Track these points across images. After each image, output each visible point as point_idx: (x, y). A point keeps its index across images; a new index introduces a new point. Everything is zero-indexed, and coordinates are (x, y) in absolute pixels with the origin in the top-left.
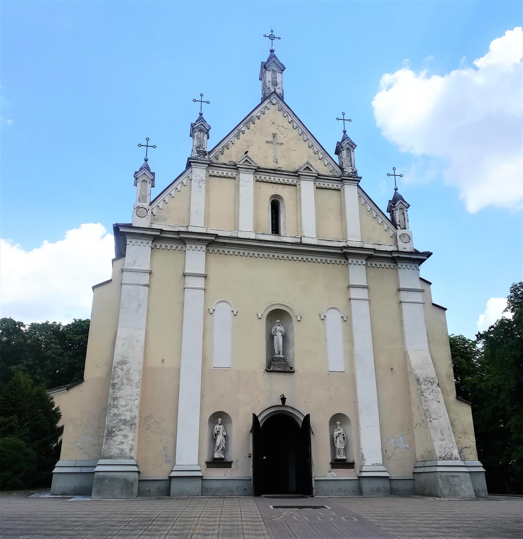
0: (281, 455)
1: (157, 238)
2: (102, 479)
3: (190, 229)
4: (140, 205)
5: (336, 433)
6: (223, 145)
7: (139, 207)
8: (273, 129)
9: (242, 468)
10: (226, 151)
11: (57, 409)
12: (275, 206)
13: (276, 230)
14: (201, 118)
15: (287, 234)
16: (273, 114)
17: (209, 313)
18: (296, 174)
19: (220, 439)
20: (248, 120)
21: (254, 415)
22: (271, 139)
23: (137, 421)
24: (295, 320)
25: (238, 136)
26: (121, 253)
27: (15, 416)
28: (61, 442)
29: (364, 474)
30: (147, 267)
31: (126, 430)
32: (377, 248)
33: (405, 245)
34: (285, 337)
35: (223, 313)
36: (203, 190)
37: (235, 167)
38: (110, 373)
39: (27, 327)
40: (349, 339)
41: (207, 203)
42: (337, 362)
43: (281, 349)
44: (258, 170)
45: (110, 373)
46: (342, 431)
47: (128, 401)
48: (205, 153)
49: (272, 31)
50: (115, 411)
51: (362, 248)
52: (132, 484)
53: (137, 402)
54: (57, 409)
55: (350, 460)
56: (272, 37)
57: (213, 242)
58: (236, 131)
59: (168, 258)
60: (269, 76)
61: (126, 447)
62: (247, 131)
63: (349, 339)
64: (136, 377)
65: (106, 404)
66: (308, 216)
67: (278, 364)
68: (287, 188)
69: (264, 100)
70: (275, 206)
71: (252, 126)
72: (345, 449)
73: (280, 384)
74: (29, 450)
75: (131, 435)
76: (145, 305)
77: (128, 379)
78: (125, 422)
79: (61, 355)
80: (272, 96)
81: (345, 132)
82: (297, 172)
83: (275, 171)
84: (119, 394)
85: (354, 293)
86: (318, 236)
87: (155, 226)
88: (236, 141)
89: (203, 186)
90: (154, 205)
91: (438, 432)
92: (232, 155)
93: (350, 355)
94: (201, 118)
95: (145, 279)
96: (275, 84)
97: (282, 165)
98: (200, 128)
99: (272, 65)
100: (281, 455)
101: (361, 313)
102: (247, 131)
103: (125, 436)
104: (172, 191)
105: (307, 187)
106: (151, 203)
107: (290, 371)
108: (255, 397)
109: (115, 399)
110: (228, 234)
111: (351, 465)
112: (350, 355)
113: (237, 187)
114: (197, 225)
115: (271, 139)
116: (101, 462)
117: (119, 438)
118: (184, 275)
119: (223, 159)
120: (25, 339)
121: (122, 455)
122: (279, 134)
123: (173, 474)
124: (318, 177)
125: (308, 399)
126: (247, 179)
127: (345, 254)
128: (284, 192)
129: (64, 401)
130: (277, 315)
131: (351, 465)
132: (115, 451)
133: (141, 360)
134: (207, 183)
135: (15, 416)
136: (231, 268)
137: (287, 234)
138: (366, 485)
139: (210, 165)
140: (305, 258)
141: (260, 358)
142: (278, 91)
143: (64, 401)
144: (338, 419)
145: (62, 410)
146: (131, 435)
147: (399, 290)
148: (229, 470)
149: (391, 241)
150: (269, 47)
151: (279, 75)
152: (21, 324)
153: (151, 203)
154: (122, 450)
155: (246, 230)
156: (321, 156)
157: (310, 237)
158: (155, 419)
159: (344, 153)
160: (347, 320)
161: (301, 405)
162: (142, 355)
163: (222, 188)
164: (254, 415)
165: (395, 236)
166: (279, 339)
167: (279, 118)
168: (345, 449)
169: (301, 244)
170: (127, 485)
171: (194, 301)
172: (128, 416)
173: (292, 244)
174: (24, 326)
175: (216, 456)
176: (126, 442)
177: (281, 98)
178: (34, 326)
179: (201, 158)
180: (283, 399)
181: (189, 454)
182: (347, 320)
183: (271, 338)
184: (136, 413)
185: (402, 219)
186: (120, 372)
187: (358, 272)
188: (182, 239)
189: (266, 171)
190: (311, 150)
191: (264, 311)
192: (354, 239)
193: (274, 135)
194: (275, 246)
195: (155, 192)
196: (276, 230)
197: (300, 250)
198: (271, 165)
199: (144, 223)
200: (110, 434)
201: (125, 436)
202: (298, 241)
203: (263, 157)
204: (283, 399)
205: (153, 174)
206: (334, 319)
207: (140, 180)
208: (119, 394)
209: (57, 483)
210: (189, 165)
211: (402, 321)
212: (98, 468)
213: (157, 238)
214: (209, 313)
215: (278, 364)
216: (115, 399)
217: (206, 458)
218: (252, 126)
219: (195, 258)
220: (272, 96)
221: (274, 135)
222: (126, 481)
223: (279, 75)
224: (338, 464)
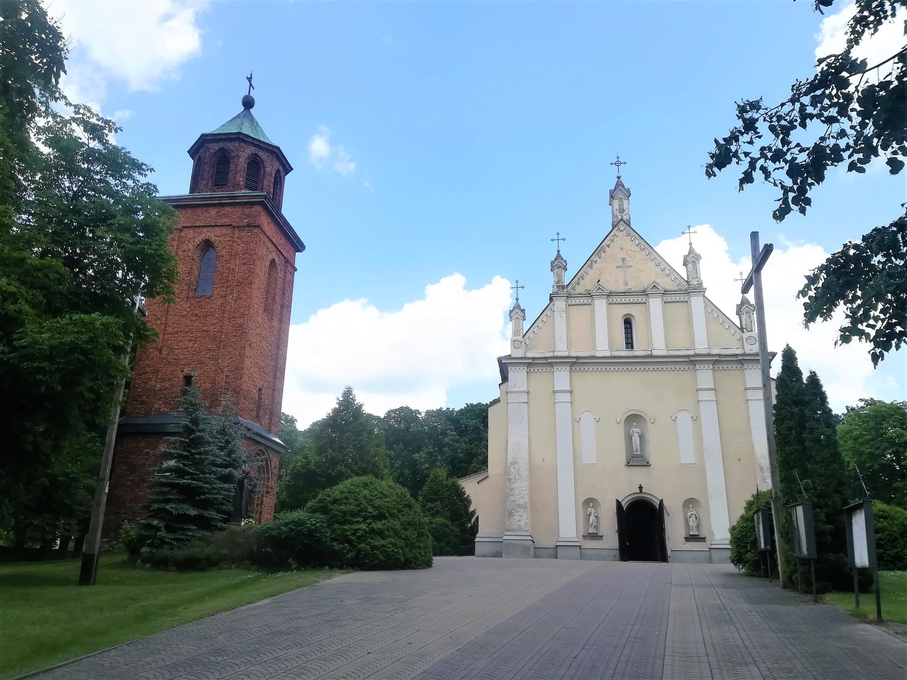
0: (641, 529)
1: (531, 364)
2: (509, 545)
3: (556, 354)
4: (516, 338)
5: (689, 514)
6: (578, 276)
7: (515, 341)
8: (622, 255)
9: (611, 540)
10: (581, 281)
11: (468, 496)
12: (628, 323)
13: (629, 344)
14: (559, 256)
15: (639, 349)
16: (622, 240)
17: (576, 421)
18: (644, 293)
19: (592, 518)
20: (599, 250)
21: (617, 501)
22: (620, 264)
23: (528, 505)
24: (649, 423)
25: (591, 266)
26: (505, 379)
27: (439, 503)
28: (478, 518)
29: (713, 546)
30: (525, 389)
31: (521, 512)
32: (724, 352)
33: (751, 347)
34: (641, 437)
35: (587, 420)
36: (564, 319)
37: (589, 295)
38: (506, 472)
39: (423, 415)
40: (698, 435)
41: (568, 330)
42: (688, 456)
43: (638, 447)
44: (610, 294)
45: (506, 472)
46: (694, 512)
47: (521, 490)
48: (563, 287)
49: (618, 157)
50: (512, 498)
51: (709, 355)
52: (529, 549)
53: (527, 492)
54: (468, 496)
55: (703, 536)
56: (618, 164)
57: (575, 363)
58: (589, 262)
59: (540, 378)
60: (616, 203)
61: (522, 523)
62: (599, 260)
63: (698, 435)
64: (525, 474)
65: (506, 494)
66: (655, 337)
67: (637, 459)
68: (638, 307)
69: (614, 227)
70: (628, 323)
71: (603, 255)
72: (698, 527)
73: (639, 476)
74: (454, 528)
75: (525, 515)
76: (526, 418)
77: (519, 475)
78: (520, 506)
79: (458, 441)
80: (621, 223)
81: (690, 244)
82: (644, 291)
83: (625, 293)
84: (514, 486)
85: (702, 396)
86: (667, 346)
87: (529, 355)
88: (590, 271)
89: (564, 315)
90: (526, 337)
91: (225, 502)
92: (587, 284)
93: (700, 451)
94: (559, 256)
95: (524, 398)
96: (622, 211)
97: (633, 286)
98: (559, 264)
99: (619, 192)
100: (641, 529)
101: (709, 413)
102: (599, 260)
103: (521, 516)
104: (539, 323)
105: (655, 303)
106: (524, 336)
107: (648, 465)
108: (622, 487)
109: (512, 490)
110: (587, 354)
111: (703, 539)
112: (700, 451)
113: (593, 311)
114: (562, 350)
115: (620, 264)
116: (506, 533)
117: (517, 518)
118: (554, 392)
119: (580, 289)
120: (422, 426)
121: (520, 529)
122: (628, 258)
123: (558, 544)
124: (666, 292)
125: (661, 488)
126: (600, 305)
127: (692, 361)
128: (636, 312)
129: (469, 486)
130: (634, 419)
131: (703, 539)
132: (515, 526)
133: (527, 461)
134: (567, 311)
135: (439, 503)
136: (592, 383)
137: (639, 349)
138: (715, 555)
139: (569, 297)
140: (656, 368)
141: (621, 457)
142: (625, 218)
143: (469, 486)
144: (690, 503)
145: (472, 498)
146: (525, 515)
147: (746, 389)
148: (601, 542)
149: (739, 345)
150: (617, 174)
151: (625, 202)
152: (418, 412)
153: (524, 336)
154: (520, 525)
155: (602, 349)
156: (668, 272)
157: (660, 348)
158: (542, 504)
159: (690, 265)
160: (696, 419)
161: (656, 492)
162: (527, 458)
163: (581, 314)
164: (617, 501)
165: (741, 339)
166: (636, 439)
167: (629, 244)
168: (698, 527)
169: (651, 356)
170: (526, 549)
171: (563, 411)
172: (522, 502)
173: (643, 357)
174: (420, 414)
175: (590, 531)
176: (522, 520)
177: (628, 224)
178: (428, 412)
179: (561, 292)
180: (641, 488)
181: (569, 528)
182: (696, 419)
183: (629, 438)
184: (527, 499)
185: (749, 322)
186: (513, 471)
187: (705, 376)
188: (550, 362)
189: (617, 294)
190: (658, 268)
191: (621, 416)
192: (701, 347)
193: (624, 260)
194: (630, 357)
195: (526, 325)
196: (629, 344)
197: (651, 361)
198: (622, 288)
199: (519, 353)
200: (511, 514)
201: (521, 516)
202: (649, 353)
203: (614, 281)
204: (641, 488)
205: (523, 311)
206: (685, 419)
207: (514, 318)
208: (514, 486)
209: (478, 548)
210: (551, 299)
211: (749, 417)
212: (505, 538)
213: (531, 364)
214: (576, 421)
215: (637, 459)
216: (512, 490)
217: (582, 533)
218: (603, 255)
219: (562, 377)
220: (621, 223)
221: (624, 260)
222: (524, 546)
223: (625, 202)
224: (691, 538)
